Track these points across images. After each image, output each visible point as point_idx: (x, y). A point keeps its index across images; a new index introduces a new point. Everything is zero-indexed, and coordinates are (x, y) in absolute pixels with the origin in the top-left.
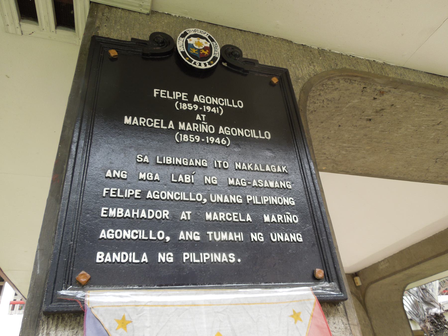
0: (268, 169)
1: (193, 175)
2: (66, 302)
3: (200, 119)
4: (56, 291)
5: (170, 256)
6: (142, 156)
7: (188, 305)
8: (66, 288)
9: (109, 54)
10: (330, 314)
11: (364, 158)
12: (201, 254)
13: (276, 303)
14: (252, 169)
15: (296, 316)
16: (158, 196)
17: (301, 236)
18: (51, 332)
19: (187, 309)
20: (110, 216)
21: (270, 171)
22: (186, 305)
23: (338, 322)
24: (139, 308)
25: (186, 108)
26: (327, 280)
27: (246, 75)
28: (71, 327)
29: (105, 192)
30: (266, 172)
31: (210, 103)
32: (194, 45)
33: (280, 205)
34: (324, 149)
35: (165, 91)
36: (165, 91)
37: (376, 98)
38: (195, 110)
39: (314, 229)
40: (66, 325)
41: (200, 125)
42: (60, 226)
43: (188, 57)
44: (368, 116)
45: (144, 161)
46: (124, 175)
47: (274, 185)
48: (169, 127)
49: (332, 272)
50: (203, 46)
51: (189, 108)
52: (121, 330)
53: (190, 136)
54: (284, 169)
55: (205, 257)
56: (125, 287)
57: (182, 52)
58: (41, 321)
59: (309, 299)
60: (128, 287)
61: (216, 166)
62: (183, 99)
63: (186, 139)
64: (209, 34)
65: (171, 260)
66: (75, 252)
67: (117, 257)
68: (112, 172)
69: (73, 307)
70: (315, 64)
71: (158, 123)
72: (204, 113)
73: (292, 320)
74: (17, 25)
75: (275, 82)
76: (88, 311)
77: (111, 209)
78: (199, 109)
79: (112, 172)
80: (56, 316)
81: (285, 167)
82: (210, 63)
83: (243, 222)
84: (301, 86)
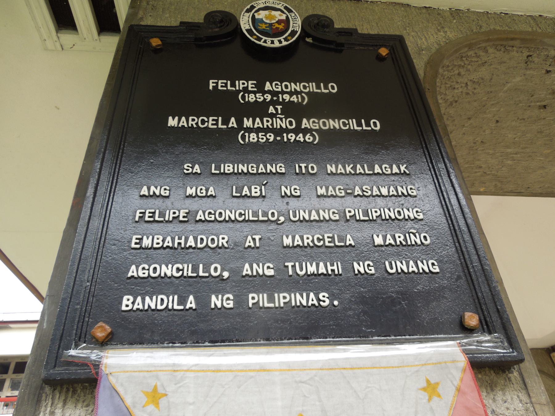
0: (377, 169)
1: (264, 185)
2: (74, 366)
3: (274, 112)
4: (62, 351)
5: (228, 299)
6: (190, 165)
7: (254, 370)
8: (76, 346)
9: (149, 44)
10: (496, 386)
11: (543, 168)
12: (276, 295)
13: (398, 367)
14: (353, 172)
15: (431, 389)
16: (213, 216)
17: (436, 263)
18: (56, 411)
19: (252, 377)
20: (143, 246)
21: (381, 172)
22: (250, 370)
23: (512, 399)
24: (179, 375)
25: (255, 99)
26: (486, 330)
27: (341, 51)
28: (85, 404)
29: (138, 215)
30: (375, 174)
31: (289, 90)
32: (264, 20)
33: (399, 220)
34: (478, 160)
35: (225, 81)
36: (225, 81)
37: (550, 71)
38: (267, 101)
39: (458, 253)
40: (78, 401)
41: (274, 119)
42: (74, 262)
43: (255, 35)
44: (541, 101)
45: (194, 171)
46: (166, 191)
47: (389, 192)
48: (230, 125)
49: (494, 315)
50: (277, 19)
51: (258, 99)
52: (151, 408)
53: (260, 134)
54: (403, 168)
55: (282, 299)
56: (162, 345)
57: (247, 30)
58: (43, 395)
59: (454, 361)
60: (166, 345)
61: (297, 171)
62: (250, 89)
63: (254, 139)
64: (285, 5)
65: (231, 304)
66: (93, 296)
67: (151, 302)
68: (149, 189)
69: (81, 373)
70: (446, 29)
71: (215, 122)
72: (280, 103)
73: (424, 396)
74: (55, 38)
75: (384, 54)
76: (103, 379)
77: (145, 238)
78: (272, 99)
79: (149, 189)
80: (65, 387)
81: (405, 166)
82: (286, 39)
83: (341, 246)
84: (426, 58)
